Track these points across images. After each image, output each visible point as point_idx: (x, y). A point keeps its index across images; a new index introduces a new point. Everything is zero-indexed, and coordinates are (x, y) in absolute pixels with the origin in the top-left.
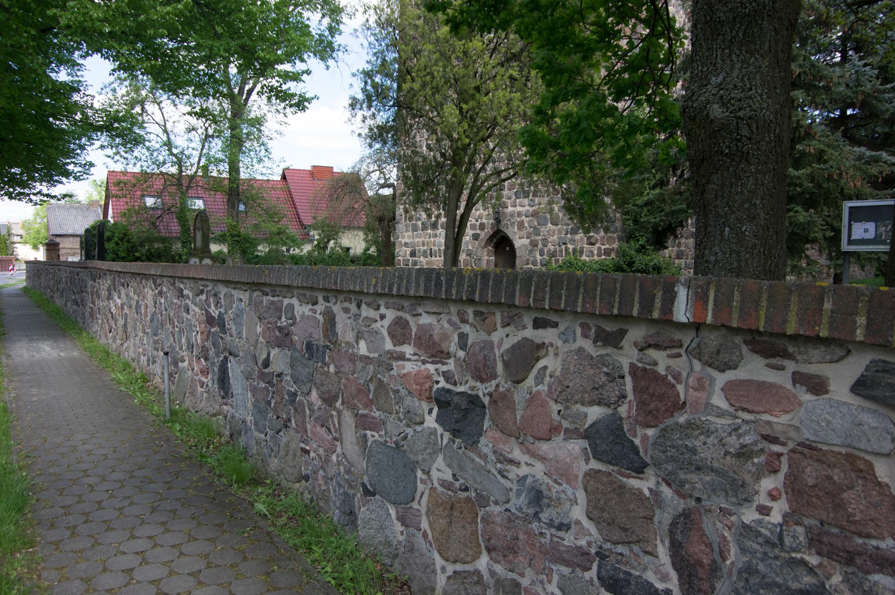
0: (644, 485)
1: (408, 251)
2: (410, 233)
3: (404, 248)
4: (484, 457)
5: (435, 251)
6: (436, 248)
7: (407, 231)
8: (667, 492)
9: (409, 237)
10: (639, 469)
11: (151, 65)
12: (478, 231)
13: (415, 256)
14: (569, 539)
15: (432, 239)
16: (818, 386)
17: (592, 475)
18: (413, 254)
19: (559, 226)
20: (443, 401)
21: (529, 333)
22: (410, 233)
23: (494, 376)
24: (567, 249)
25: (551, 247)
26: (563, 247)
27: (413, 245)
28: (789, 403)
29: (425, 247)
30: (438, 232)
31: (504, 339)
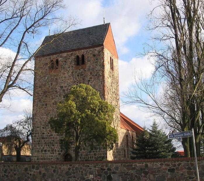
0: (192, 171)
1: (36, 158)
2: (37, 153)
3: (34, 158)
4: (176, 173)
5: (46, 158)
6: (46, 157)
7: (36, 152)
8: (194, 170)
9: (36, 154)
10: (191, 169)
11: (65, 122)
12: (60, 152)
13: (38, 160)
14: (186, 177)
15: (44, 155)
16: (202, 162)
17: (187, 171)
18: (38, 159)
19: (86, 151)
20: (169, 170)
21: (180, 162)
22: (37, 153)
23: (176, 166)
24: (88, 157)
25: (83, 156)
26: (87, 156)
27: (38, 156)
28: (200, 163)
29: (42, 157)
30: (47, 153)
31: (177, 163)
